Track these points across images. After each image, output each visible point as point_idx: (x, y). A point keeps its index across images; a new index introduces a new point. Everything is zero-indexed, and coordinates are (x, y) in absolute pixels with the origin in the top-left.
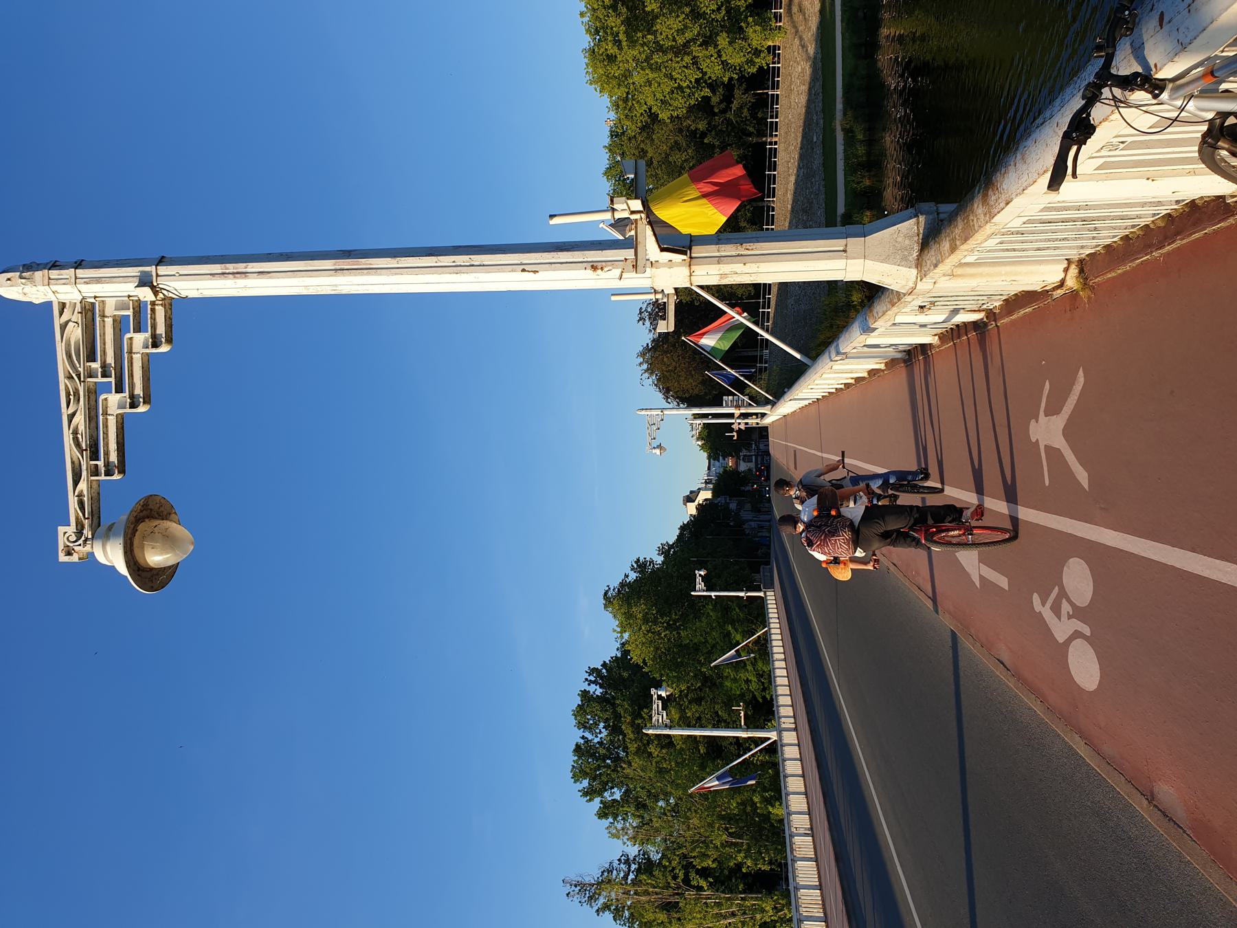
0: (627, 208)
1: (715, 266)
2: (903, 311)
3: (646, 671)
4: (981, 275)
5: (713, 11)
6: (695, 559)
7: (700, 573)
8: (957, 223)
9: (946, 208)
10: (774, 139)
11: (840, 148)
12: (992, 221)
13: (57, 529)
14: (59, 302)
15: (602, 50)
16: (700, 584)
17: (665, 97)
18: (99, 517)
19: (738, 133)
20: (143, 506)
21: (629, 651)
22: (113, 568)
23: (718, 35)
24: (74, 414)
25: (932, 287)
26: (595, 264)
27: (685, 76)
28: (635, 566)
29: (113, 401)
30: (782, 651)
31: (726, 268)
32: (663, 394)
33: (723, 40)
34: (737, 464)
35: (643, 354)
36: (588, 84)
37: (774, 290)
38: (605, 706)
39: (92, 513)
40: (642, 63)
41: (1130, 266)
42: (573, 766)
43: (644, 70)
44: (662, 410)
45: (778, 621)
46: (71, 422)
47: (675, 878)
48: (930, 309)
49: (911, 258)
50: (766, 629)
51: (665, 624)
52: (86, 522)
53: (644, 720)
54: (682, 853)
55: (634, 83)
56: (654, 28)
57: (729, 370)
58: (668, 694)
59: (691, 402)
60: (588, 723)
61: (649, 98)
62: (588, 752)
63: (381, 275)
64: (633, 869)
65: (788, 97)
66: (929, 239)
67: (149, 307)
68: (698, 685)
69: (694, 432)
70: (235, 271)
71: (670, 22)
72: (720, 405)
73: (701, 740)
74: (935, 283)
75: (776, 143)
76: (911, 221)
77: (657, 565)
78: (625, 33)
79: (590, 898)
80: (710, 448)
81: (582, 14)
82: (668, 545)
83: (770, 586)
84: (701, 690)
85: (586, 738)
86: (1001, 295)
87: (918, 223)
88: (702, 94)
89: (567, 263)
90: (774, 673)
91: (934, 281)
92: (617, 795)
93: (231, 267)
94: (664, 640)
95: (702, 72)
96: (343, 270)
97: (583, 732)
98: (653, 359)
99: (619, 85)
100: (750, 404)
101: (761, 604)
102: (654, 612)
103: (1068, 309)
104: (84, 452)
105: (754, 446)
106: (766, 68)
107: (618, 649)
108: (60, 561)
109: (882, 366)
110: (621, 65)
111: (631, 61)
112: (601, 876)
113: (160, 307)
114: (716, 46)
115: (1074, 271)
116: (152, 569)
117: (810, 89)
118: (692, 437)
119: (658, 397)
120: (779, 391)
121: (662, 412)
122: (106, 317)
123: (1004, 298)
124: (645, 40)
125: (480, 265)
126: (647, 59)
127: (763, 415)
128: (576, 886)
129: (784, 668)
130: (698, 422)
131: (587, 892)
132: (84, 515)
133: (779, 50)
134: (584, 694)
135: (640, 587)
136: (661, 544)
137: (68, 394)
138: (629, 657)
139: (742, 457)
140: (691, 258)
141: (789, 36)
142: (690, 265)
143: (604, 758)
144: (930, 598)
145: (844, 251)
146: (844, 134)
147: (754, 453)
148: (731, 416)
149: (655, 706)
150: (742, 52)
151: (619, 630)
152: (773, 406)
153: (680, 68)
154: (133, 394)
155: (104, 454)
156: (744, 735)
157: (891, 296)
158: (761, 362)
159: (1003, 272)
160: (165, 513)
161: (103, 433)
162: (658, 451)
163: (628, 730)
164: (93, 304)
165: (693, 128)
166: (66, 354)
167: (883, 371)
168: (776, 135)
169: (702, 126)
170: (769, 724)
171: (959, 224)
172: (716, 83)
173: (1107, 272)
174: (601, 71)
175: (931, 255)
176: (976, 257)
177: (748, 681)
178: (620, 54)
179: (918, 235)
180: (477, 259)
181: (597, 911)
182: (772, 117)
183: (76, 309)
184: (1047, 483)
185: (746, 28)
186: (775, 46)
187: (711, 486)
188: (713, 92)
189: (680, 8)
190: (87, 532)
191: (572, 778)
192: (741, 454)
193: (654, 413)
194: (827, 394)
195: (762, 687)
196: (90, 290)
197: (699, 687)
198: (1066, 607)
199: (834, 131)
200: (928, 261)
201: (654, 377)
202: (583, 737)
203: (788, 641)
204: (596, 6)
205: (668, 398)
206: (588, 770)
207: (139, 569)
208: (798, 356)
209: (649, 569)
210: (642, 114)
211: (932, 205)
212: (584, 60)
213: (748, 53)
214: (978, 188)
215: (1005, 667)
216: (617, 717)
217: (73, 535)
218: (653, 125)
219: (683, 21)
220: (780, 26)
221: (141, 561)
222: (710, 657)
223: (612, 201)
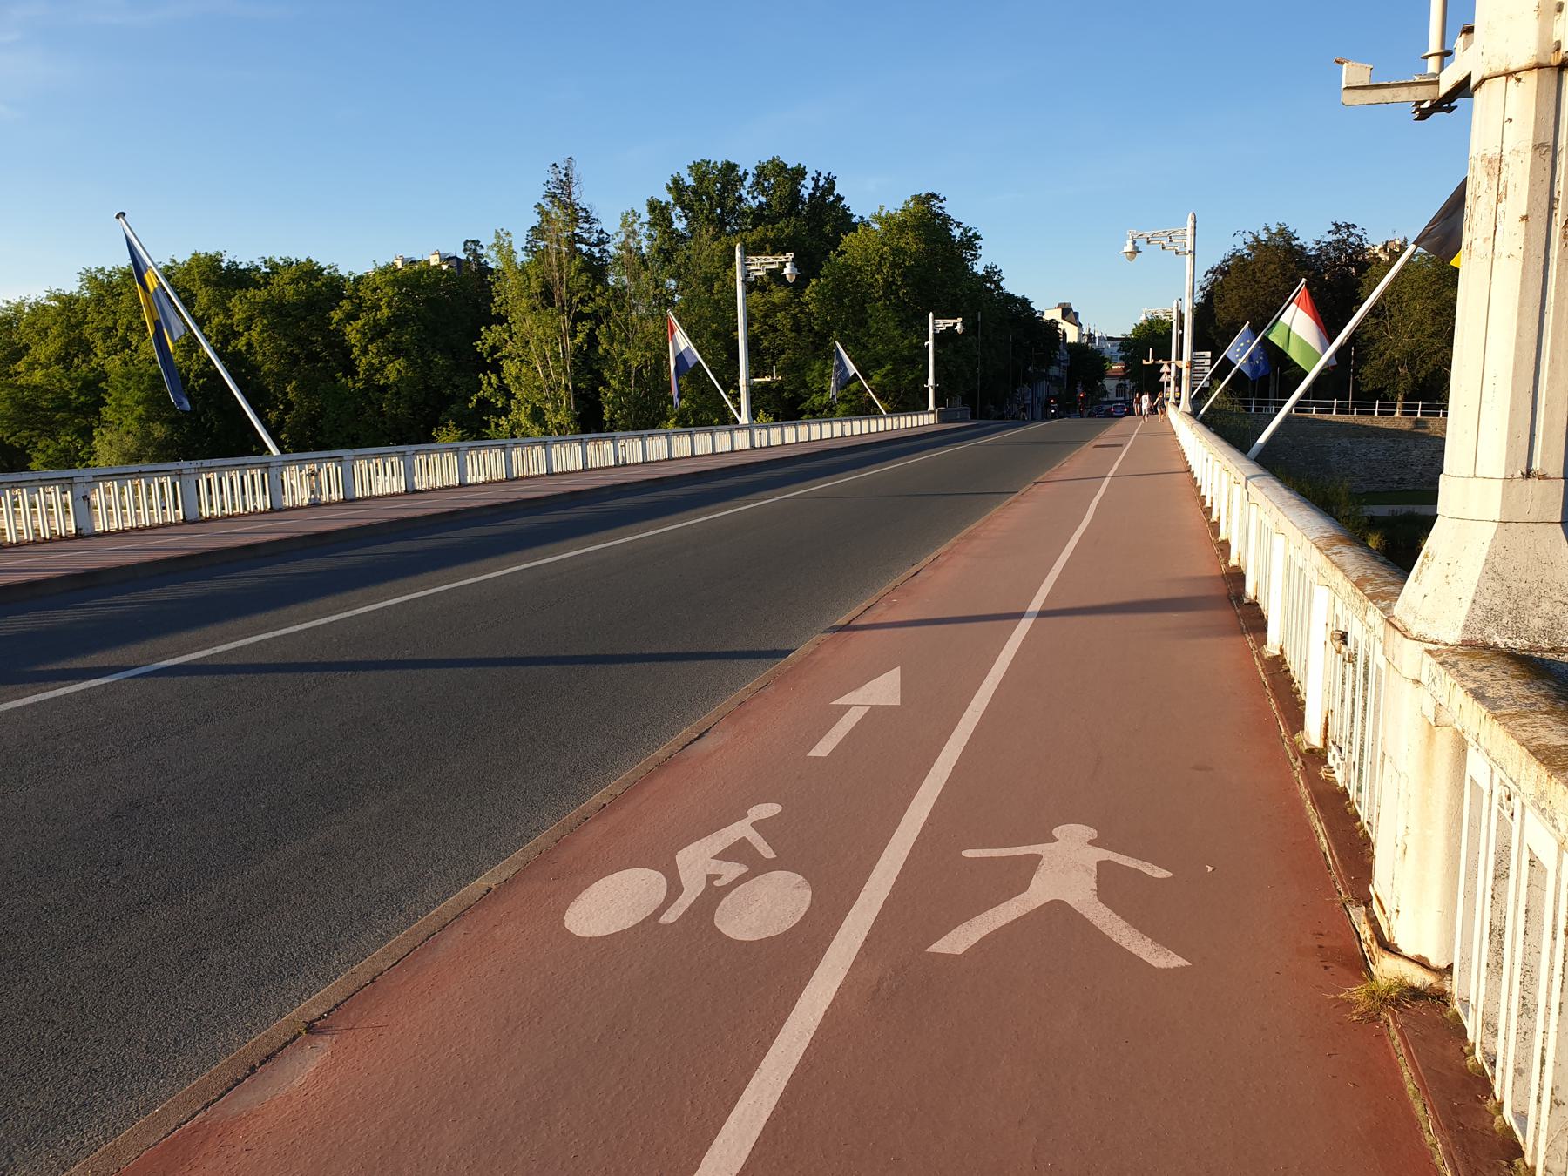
1: (1531, 138)
2: (1339, 602)
6: (979, 319)
16: (943, 324)
25: (1406, 673)
28: (970, 234)
30: (855, 433)
32: (1219, 266)
35: (1283, 232)
38: (787, 202)
41: (1435, 1145)
42: (709, 162)
45: (895, 428)
47: (582, 301)
48: (1339, 652)
49: (1490, 630)
50: (885, 413)
51: (891, 280)
54: (611, 310)
58: (788, 277)
59: (1203, 314)
60: (765, 180)
62: (728, 182)
64: (592, 249)
68: (816, 327)
79: (554, 195)
82: (1000, 281)
83: (943, 418)
84: (810, 331)
85: (745, 178)
86: (1359, 790)
91: (1424, 680)
92: (680, 225)
94: (872, 278)
97: (753, 174)
98: (1274, 249)
100: (1193, 389)
101: (919, 406)
103: (1326, 942)
112: (581, 208)
115: (1419, 978)
121: (1190, 252)
123: (1350, 792)
128: (566, 175)
129: (821, 435)
131: (560, 191)
134: (800, 173)
136: (1001, 271)
143: (721, 205)
148: (1180, 357)
151: (883, 214)
152: (1191, 414)
156: (742, 382)
157: (1378, 580)
158: (1258, 403)
162: (1129, 248)
167: (1226, 562)
170: (771, 419)
173: (1415, 1068)
179: (1553, 650)
181: (539, 205)
184: (968, 854)
191: (694, 162)
193: (1189, 241)
194: (1198, 484)
198: (732, 870)
201: (1246, 251)
202: (746, 174)
205: (1214, 273)
206: (706, 183)
208: (1262, 439)
216: (774, 220)
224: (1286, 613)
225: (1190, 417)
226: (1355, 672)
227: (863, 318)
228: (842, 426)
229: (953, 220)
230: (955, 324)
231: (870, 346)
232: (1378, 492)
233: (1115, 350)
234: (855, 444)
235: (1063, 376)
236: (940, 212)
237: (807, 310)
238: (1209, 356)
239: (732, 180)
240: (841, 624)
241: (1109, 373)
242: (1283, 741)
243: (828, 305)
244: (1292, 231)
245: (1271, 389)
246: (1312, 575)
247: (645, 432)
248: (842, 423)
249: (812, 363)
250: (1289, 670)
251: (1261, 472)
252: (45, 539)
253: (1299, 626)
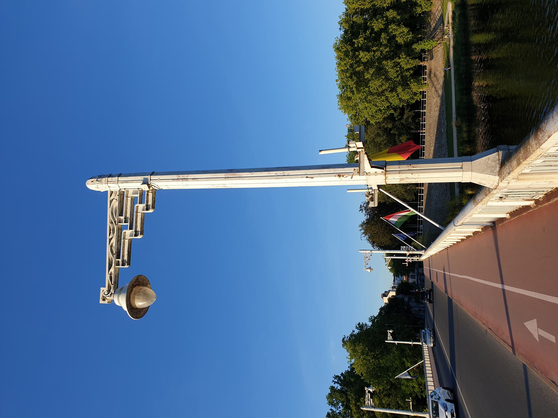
0: (355, 146)
2: (491, 199)
3: (363, 379)
4: (533, 179)
5: (395, 77)
6: (387, 325)
7: (390, 331)
8: (521, 151)
9: (512, 147)
10: (424, 131)
11: (455, 134)
12: (541, 147)
13: (100, 289)
14: (111, 191)
15: (345, 95)
16: (390, 337)
17: (373, 114)
18: (118, 284)
19: (406, 128)
20: (136, 280)
21: (354, 368)
22: (121, 307)
23: (397, 87)
24: (111, 239)
26: (340, 174)
27: (382, 105)
29: (128, 233)
31: (403, 176)
33: (399, 89)
34: (408, 279)
35: (362, 226)
36: (339, 110)
37: (425, 189)
38: (342, 395)
39: (115, 282)
40: (363, 100)
43: (364, 103)
44: (371, 251)
45: (429, 357)
46: (110, 242)
48: (505, 199)
49: (495, 171)
50: (423, 361)
51: (372, 356)
52: (112, 286)
53: (361, 403)
55: (359, 109)
56: (369, 85)
57: (404, 233)
58: (373, 390)
60: (334, 402)
61: (366, 115)
63: (244, 180)
65: (430, 113)
66: (503, 163)
67: (146, 193)
68: (389, 387)
69: (387, 263)
70: (183, 178)
71: (376, 82)
72: (399, 249)
73: (390, 416)
74: (508, 183)
75: (424, 133)
76: (495, 154)
77: (368, 326)
78: (355, 87)
80: (395, 271)
81: (337, 81)
85: (333, 410)
86: (543, 191)
87: (499, 155)
88: (390, 112)
89: (327, 174)
90: (427, 384)
91: (508, 182)
93: (181, 176)
94: (372, 364)
95: (390, 103)
96: (229, 177)
97: (331, 407)
98: (367, 228)
99: (353, 109)
100: (414, 250)
102: (367, 350)
104: (114, 255)
105: (416, 271)
106: (419, 100)
107: (349, 367)
108: (100, 303)
109: (480, 230)
110: (353, 101)
111: (358, 99)
113: (151, 193)
114: (396, 92)
116: (137, 309)
117: (440, 109)
118: (386, 265)
119: (369, 246)
120: (428, 244)
121: (371, 251)
122: (128, 197)
124: (364, 90)
125: (287, 175)
126: (365, 98)
127: (421, 255)
129: (432, 381)
130: (389, 258)
132: (111, 283)
133: (425, 93)
134: (332, 388)
135: (360, 337)
136: (371, 316)
137: (110, 230)
138: (354, 371)
139: (410, 276)
140: (386, 171)
141: (430, 87)
142: (385, 174)
144: (510, 346)
145: (461, 168)
146: (457, 128)
147: (416, 274)
148: (405, 255)
149: (367, 396)
150: (408, 94)
151: (349, 357)
152: (425, 251)
153: (380, 101)
154: (136, 230)
155: (122, 256)
157: (485, 191)
158: (419, 231)
159: (545, 178)
160: (145, 284)
161: (123, 247)
162: (369, 270)
163: (354, 408)
164: (124, 192)
165: (386, 127)
166: (111, 213)
167: (481, 232)
168: (424, 129)
169: (390, 126)
170: (425, 410)
171: (522, 151)
172: (396, 107)
174: (345, 104)
175: (506, 168)
176: (531, 170)
177: (413, 387)
178: (353, 96)
179: (499, 160)
180: (286, 173)
182: (422, 122)
183: (117, 194)
185: (410, 84)
186: (423, 91)
187: (395, 289)
188: (395, 111)
189: (380, 76)
190: (112, 291)
192: (410, 274)
194: (452, 245)
195: (421, 391)
196: (123, 186)
197: (389, 388)
199: (452, 127)
200: (504, 172)
201: (367, 236)
202: (331, 410)
204: (343, 77)
205: (374, 246)
207: (132, 308)
208: (438, 226)
209: (364, 328)
210: (362, 121)
211: (506, 146)
212: (336, 100)
213: (411, 94)
214: (531, 133)
215: (556, 385)
216: (348, 400)
217: (106, 291)
218: (367, 126)
219: (382, 82)
220: (426, 83)
221: (133, 305)
222: (394, 373)
223: (348, 143)
224: (496, 213)
225: (426, 251)
226: (510, 195)
227: (386, 368)
228: (428, 377)
229: (352, 333)
230: (390, 333)
231: (396, 366)
232: (450, 192)
233: (398, 279)
234: (436, 371)
235: (408, 297)
236: (349, 338)
237: (382, 390)
238: (405, 247)
239: (333, 415)
240: (512, 350)
241: (406, 280)
242: (534, 210)
243: (380, 382)
244: (361, 223)
245: (414, 227)
246: (484, 206)
248: (428, 377)
249: (402, 390)
250: (514, 211)
251: (453, 222)
253: (499, 209)
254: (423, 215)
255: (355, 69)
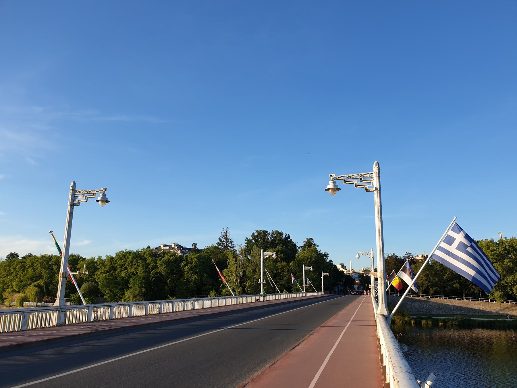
10: (464, 299)
16: (325, 274)
28: (326, 253)
34: (357, 284)
35: (394, 255)
45: (300, 296)
65: (478, 304)
81: (506, 238)
121: (376, 189)
129: (270, 299)
133: (495, 302)
139: (360, 286)
149: (309, 267)
158: (462, 298)
203: (259, 304)
230: (327, 274)
236: (313, 242)
247: (185, 300)
252: (6, 332)
254: (405, 296)
255: (513, 252)
